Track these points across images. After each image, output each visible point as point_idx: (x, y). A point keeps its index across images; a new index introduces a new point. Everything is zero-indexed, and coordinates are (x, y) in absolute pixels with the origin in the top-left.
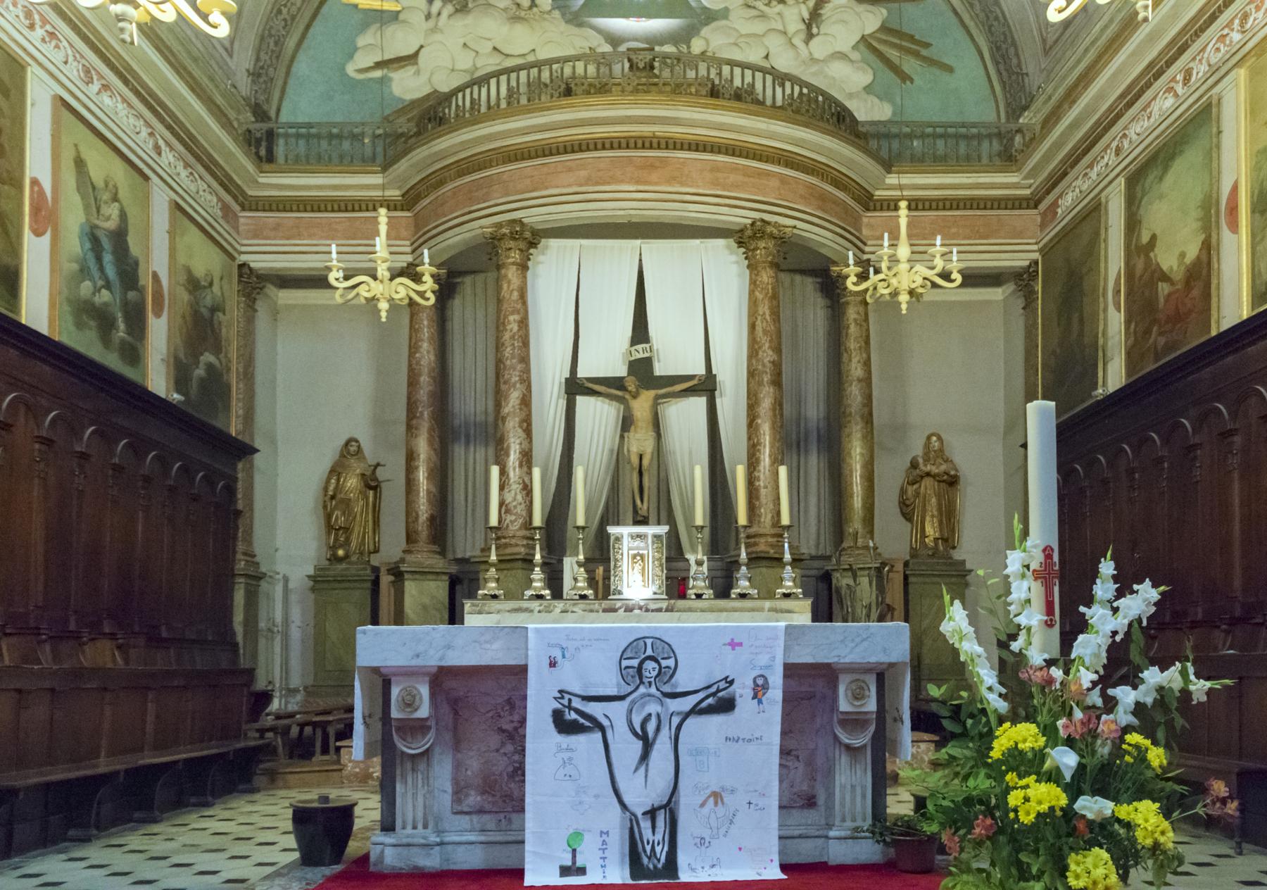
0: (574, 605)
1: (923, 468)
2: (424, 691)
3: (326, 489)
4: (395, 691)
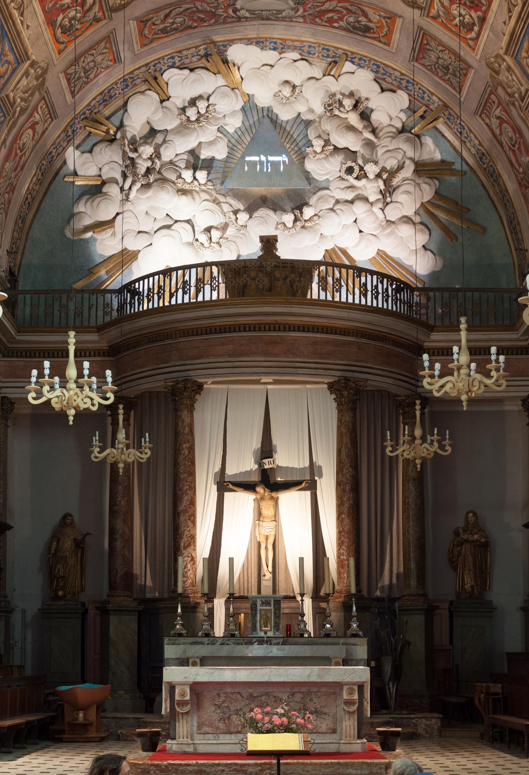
0: (228, 640)
1: (462, 536)
2: (188, 691)
3: (50, 549)
4: (177, 691)
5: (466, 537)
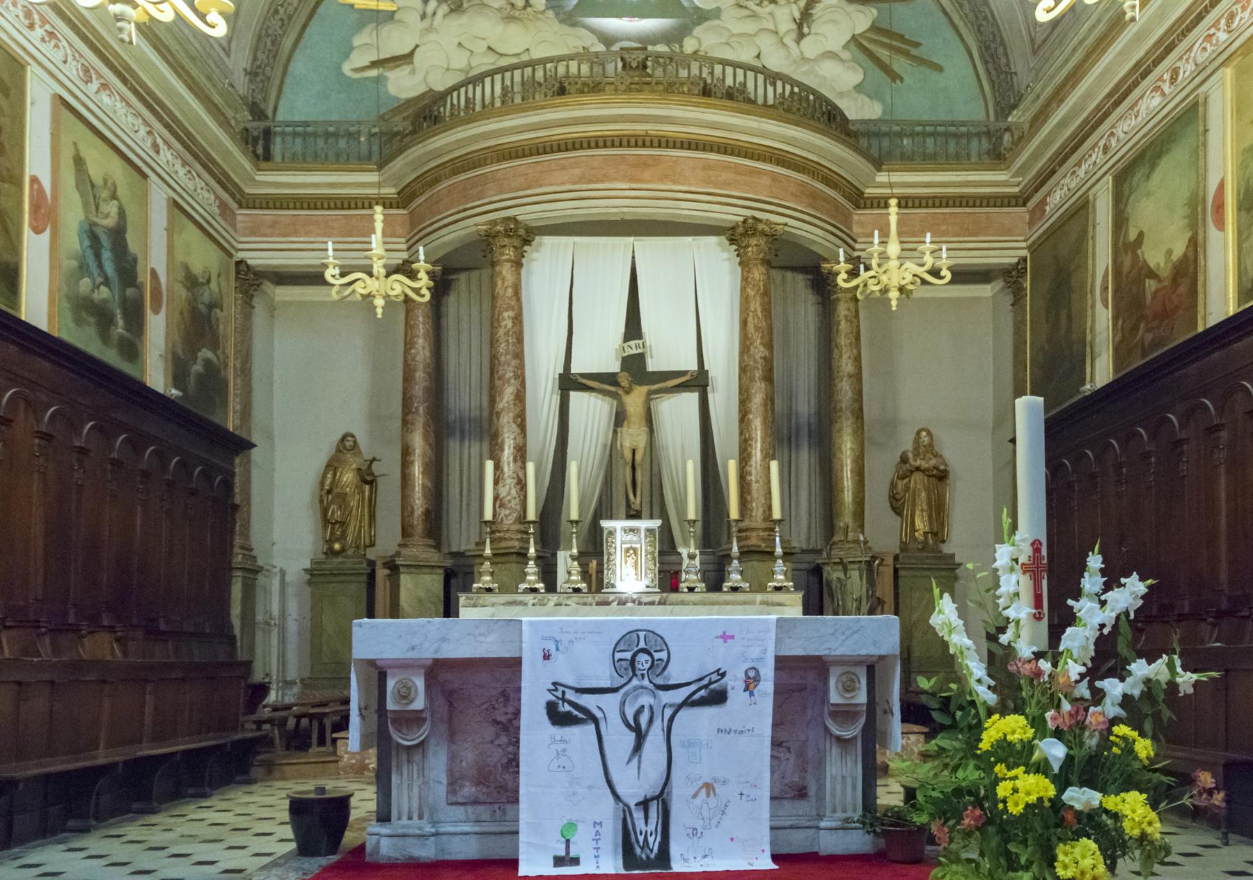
0: (568, 598)
1: (913, 463)
2: (420, 683)
3: (322, 484)
4: (391, 684)
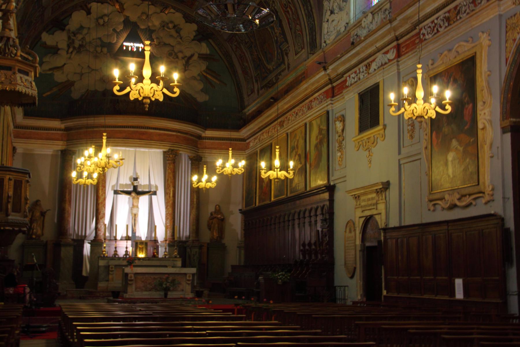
5: (215, 216)
